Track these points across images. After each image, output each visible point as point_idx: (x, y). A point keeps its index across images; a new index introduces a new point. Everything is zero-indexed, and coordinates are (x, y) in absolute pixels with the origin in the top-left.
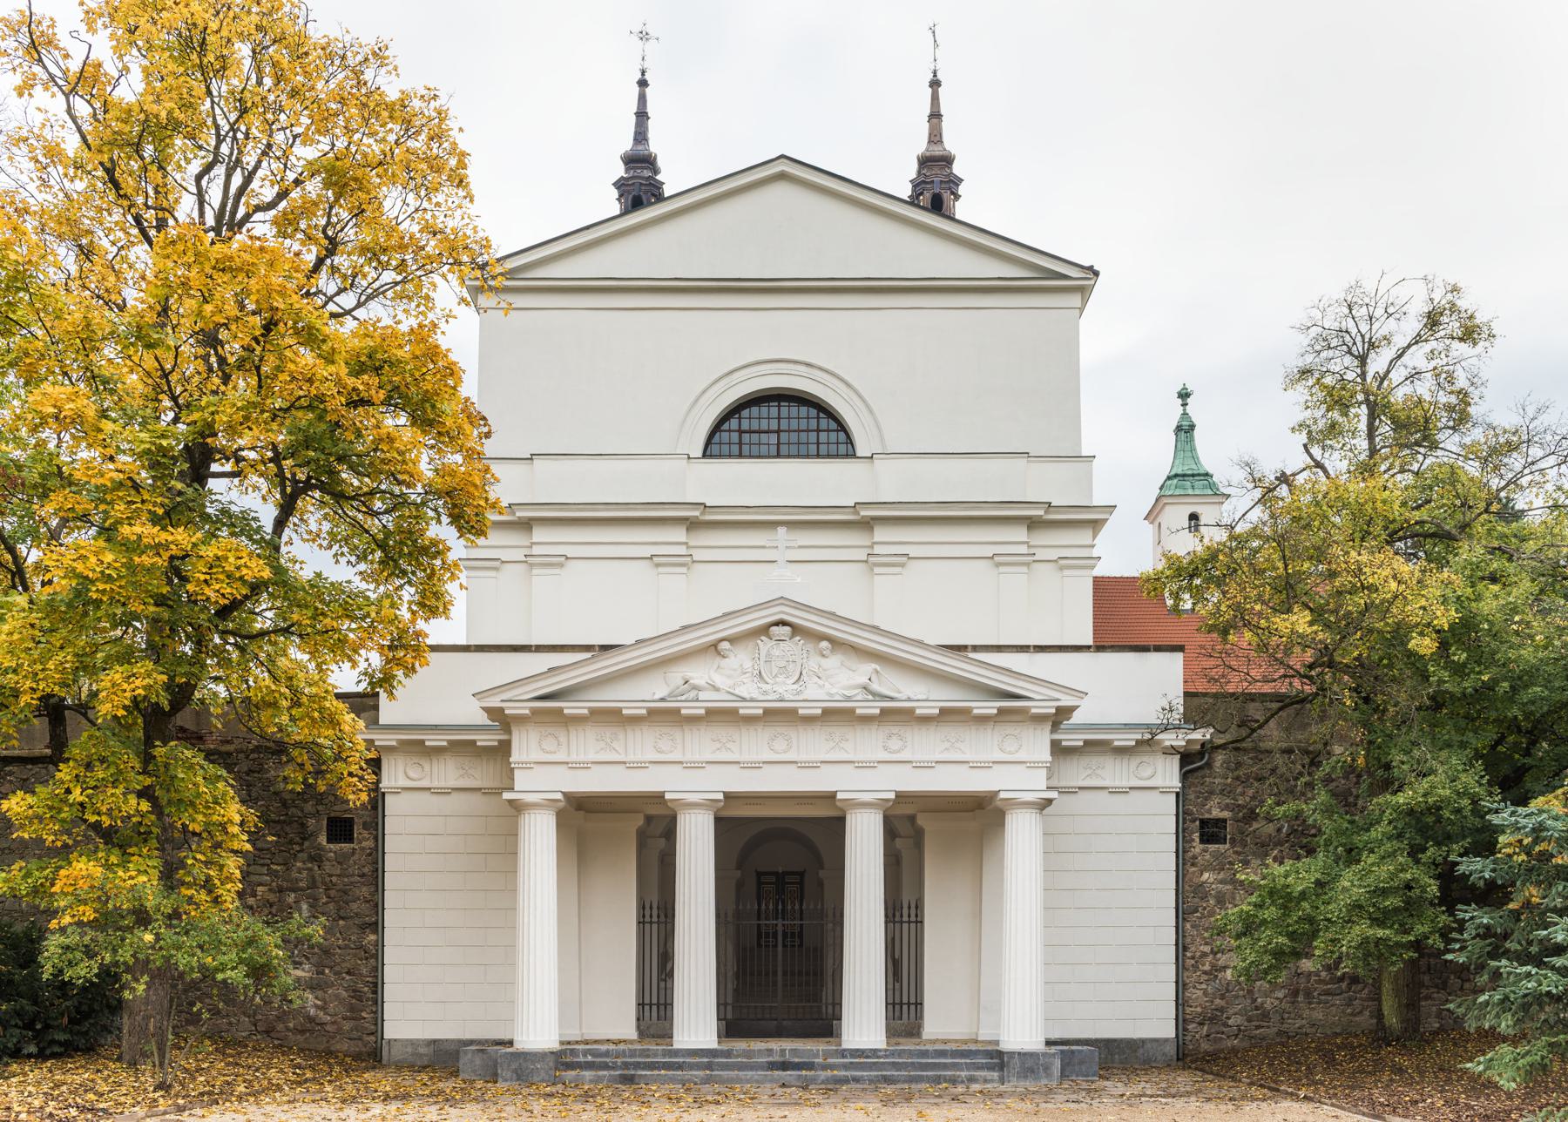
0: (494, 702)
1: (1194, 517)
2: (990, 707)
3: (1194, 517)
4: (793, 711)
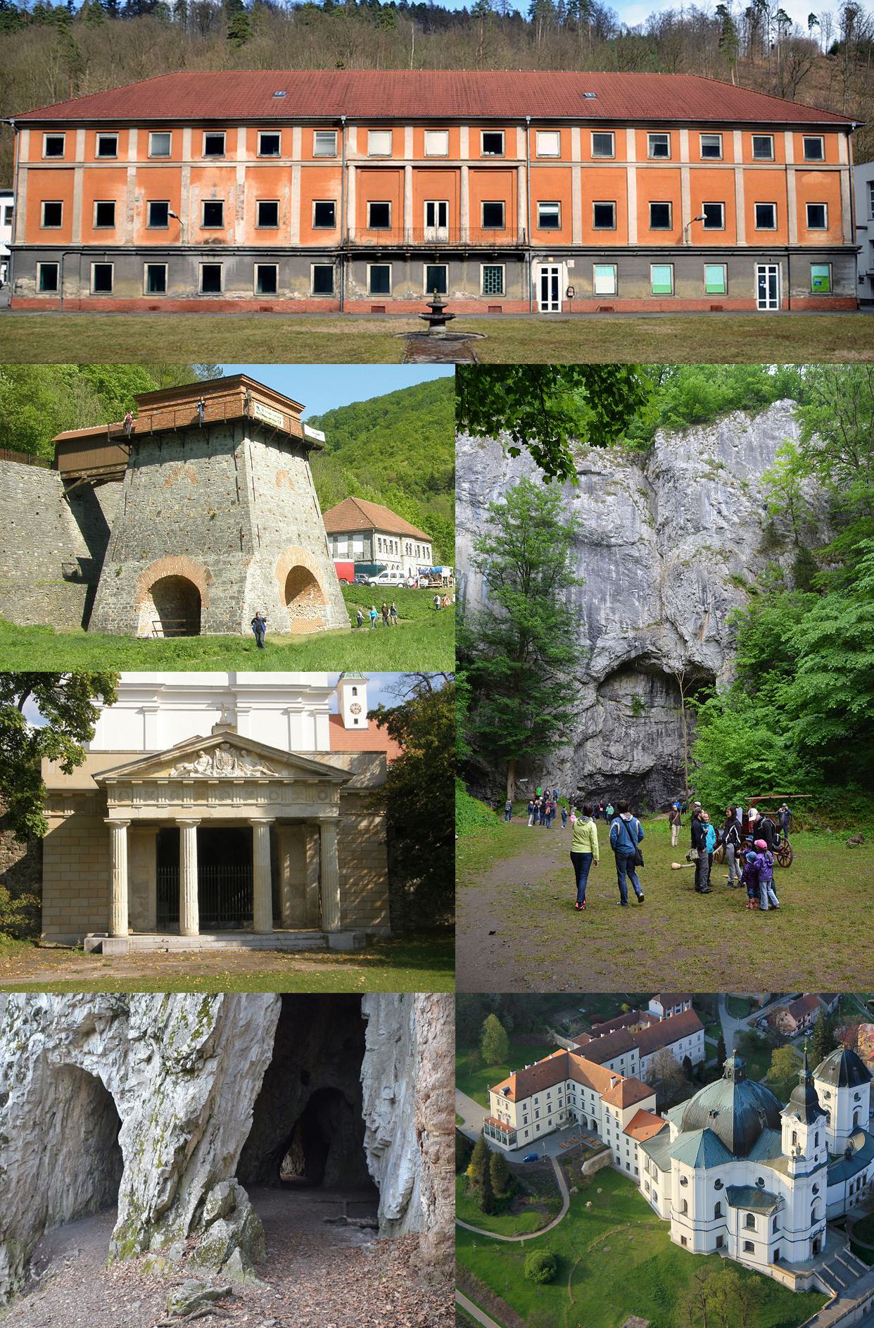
0: (100, 778)
1: (354, 689)
2: (315, 780)
3: (354, 689)
4: (256, 782)
